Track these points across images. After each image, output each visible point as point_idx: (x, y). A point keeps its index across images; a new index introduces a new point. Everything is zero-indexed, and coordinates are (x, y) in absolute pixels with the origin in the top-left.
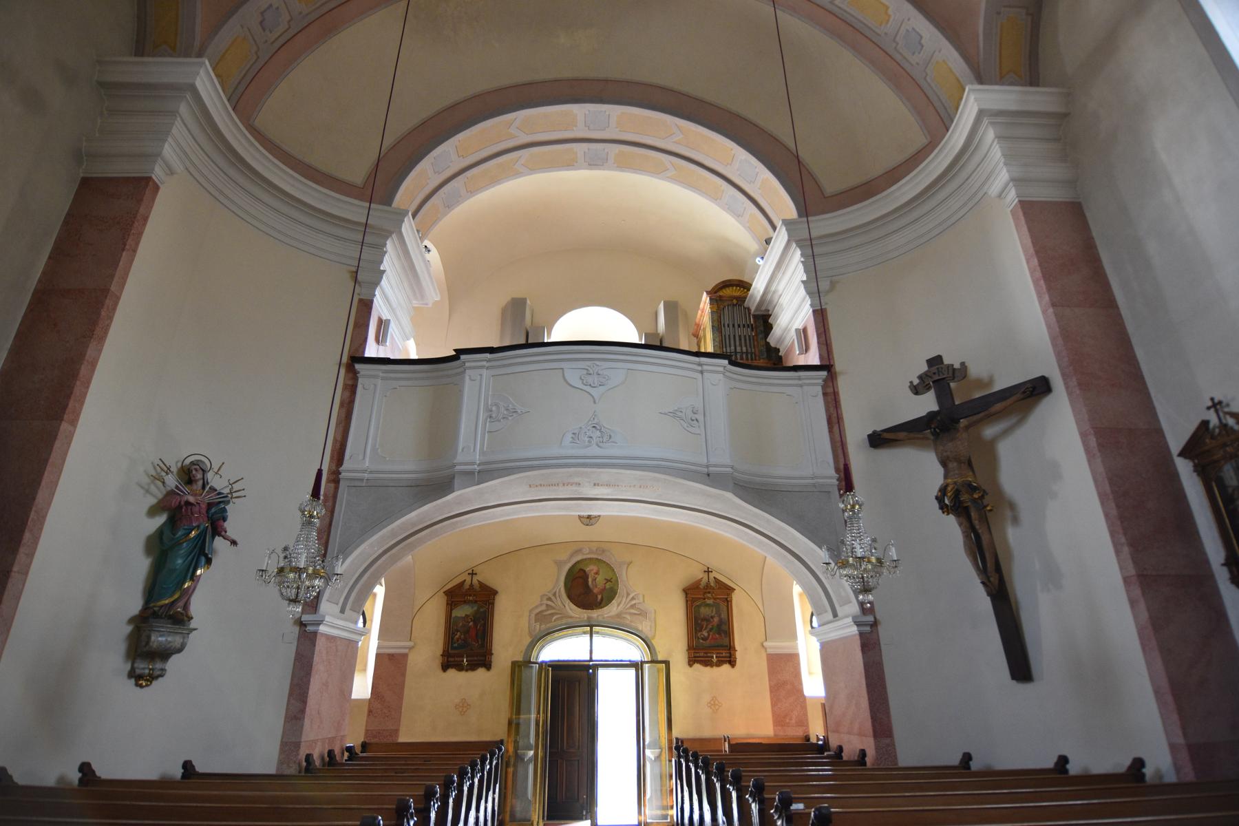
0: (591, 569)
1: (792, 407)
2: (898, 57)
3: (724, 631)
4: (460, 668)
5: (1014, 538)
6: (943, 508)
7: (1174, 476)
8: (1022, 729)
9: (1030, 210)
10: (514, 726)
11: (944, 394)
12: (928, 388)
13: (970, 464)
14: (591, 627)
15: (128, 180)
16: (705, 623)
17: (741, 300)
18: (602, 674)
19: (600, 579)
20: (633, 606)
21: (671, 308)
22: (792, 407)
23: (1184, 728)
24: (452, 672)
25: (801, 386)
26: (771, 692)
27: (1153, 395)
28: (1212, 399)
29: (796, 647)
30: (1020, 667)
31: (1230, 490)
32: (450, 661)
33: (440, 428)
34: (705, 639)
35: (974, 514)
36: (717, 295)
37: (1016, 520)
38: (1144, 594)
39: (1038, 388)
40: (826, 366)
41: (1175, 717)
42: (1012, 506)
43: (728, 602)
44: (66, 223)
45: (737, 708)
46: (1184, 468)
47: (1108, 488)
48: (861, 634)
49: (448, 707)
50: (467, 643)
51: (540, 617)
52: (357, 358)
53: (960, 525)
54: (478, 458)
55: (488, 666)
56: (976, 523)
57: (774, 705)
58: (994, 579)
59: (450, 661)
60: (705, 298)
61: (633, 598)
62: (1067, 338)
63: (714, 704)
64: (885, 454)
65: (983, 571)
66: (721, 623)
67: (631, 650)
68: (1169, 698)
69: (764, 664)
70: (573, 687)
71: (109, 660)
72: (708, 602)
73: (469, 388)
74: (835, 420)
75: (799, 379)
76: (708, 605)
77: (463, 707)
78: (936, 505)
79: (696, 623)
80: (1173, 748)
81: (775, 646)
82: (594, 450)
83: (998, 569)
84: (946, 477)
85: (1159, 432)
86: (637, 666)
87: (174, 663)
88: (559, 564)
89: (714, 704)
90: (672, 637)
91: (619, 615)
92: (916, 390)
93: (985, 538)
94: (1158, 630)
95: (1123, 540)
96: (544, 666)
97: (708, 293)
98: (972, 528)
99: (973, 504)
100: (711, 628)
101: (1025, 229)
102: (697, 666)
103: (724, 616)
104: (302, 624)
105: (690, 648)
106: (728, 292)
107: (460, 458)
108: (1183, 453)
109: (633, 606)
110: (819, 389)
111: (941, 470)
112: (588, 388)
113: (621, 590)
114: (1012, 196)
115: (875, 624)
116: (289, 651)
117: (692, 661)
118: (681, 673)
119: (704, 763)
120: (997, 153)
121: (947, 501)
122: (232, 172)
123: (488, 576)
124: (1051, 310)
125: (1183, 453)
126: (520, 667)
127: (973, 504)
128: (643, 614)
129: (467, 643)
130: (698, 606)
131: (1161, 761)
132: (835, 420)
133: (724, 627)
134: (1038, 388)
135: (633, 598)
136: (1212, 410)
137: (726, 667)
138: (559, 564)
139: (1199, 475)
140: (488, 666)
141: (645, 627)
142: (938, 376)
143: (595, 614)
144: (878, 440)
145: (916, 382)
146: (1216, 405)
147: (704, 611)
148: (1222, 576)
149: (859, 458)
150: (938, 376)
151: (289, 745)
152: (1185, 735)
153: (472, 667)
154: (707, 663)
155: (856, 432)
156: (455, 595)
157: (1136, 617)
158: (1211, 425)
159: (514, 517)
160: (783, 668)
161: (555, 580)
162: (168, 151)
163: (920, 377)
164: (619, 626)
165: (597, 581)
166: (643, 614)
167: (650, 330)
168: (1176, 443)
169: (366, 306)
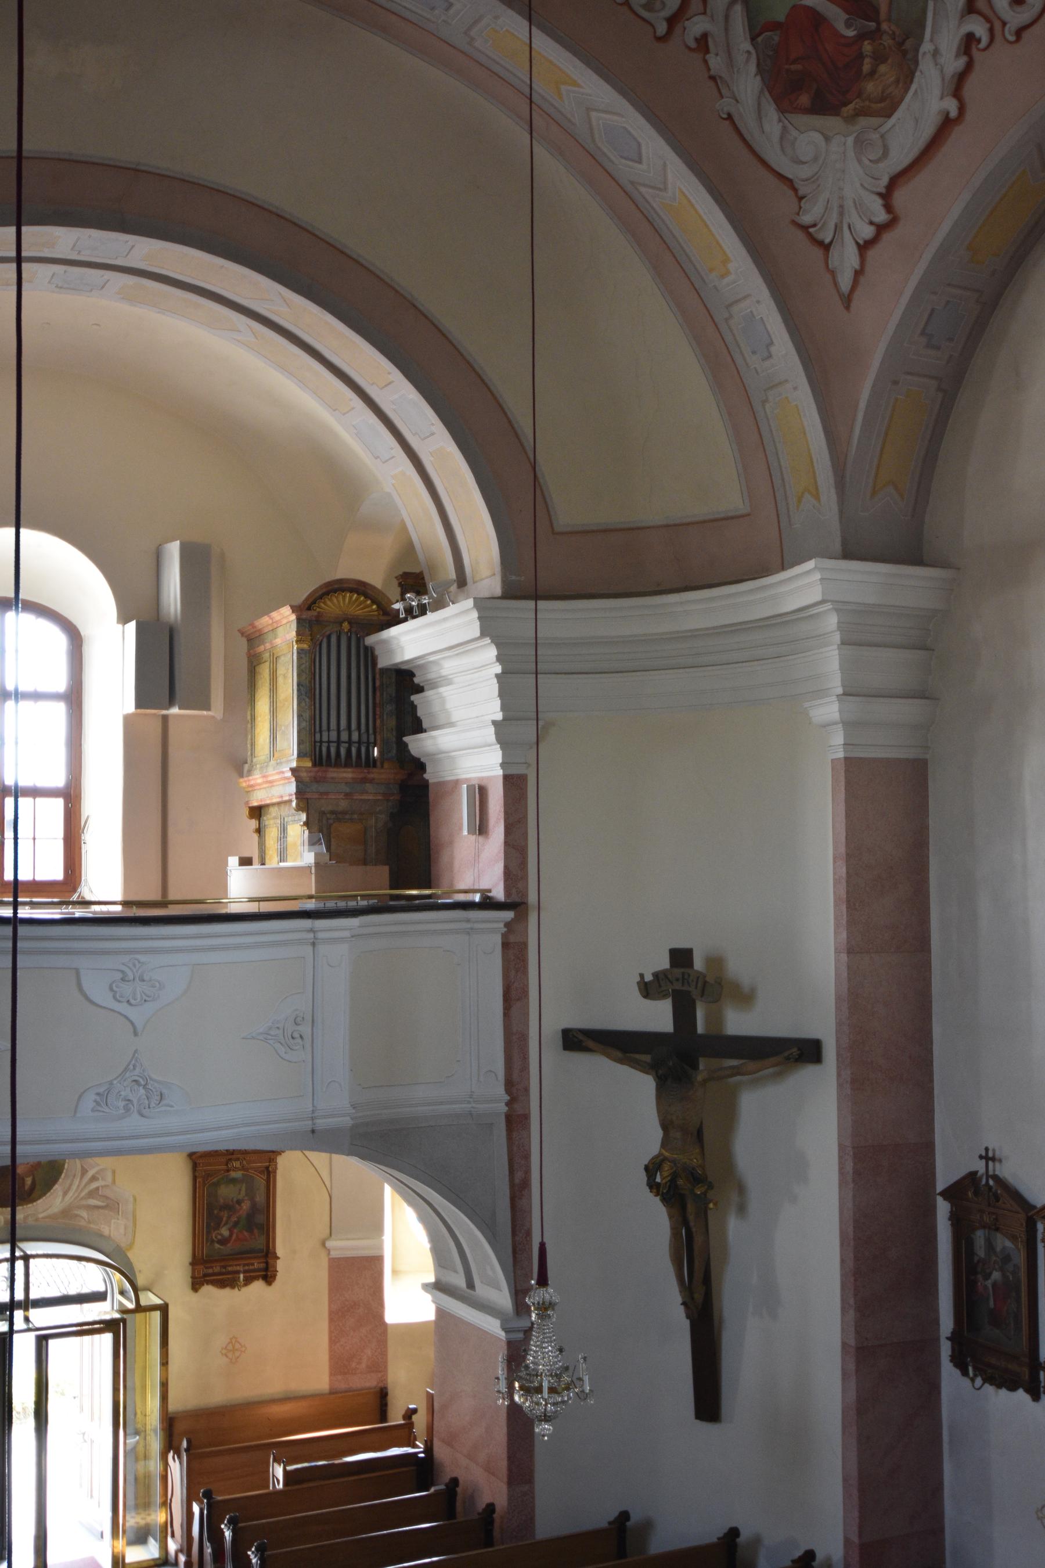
1: (448, 964)
2: (729, 338)
3: (260, 1222)
5: (736, 1231)
6: (652, 1185)
7: (932, 1210)
8: (695, 1482)
9: (856, 773)
11: (683, 1013)
12: (661, 996)
13: (699, 1134)
16: (225, 1215)
20: (93, 1194)
21: (196, 560)
23: (861, 1527)
25: (469, 932)
26: (331, 1320)
27: (936, 1092)
28: (987, 1149)
29: (381, 1247)
30: (708, 1404)
31: (976, 1259)
34: (223, 1242)
35: (690, 1208)
37: (742, 1209)
38: (857, 1371)
39: (808, 1051)
41: (856, 1514)
42: (741, 1189)
45: (271, 1346)
46: (943, 1208)
47: (850, 1230)
48: (510, 1343)
53: (671, 1217)
56: (691, 1218)
57: (333, 1341)
58: (699, 1297)
61: (94, 1178)
62: (854, 1000)
63: (233, 1349)
65: (687, 1289)
66: (254, 1209)
68: (855, 1492)
72: (233, 1174)
75: (468, 921)
76: (234, 1181)
78: (643, 1177)
79: (210, 1213)
80: (847, 1541)
81: (342, 1246)
82: (134, 1123)
83: (707, 1280)
84: (664, 1145)
85: (929, 1147)
89: (233, 1349)
91: (66, 1213)
92: (649, 989)
93: (698, 1239)
94: (864, 1411)
95: (852, 1301)
97: (294, 609)
98: (685, 1223)
99: (692, 1187)
100: (232, 1227)
101: (842, 796)
102: (208, 1289)
103: (260, 1198)
105: (196, 1261)
108: (946, 1194)
109: (93, 1194)
110: (498, 939)
111: (660, 1133)
112: (123, 1008)
114: (836, 744)
117: (196, 1285)
119: (207, 1442)
121: (658, 1179)
124: (844, 957)
125: (946, 1194)
127: (692, 1187)
128: (112, 1206)
130: (217, 1185)
132: (514, 995)
133: (260, 1218)
134: (808, 1051)
135: (94, 1178)
136: (984, 1161)
137: (258, 1285)
139: (952, 1225)
141: (114, 1229)
142: (682, 979)
144: (574, 1040)
145: (648, 978)
146: (988, 1157)
147: (227, 1192)
148: (946, 1349)
150: (682, 979)
152: (860, 1536)
154: (226, 1281)
157: (844, 1391)
158: (979, 1174)
160: (357, 1281)
163: (656, 975)
164: (64, 1231)
166: (112, 1206)
168: (945, 1177)
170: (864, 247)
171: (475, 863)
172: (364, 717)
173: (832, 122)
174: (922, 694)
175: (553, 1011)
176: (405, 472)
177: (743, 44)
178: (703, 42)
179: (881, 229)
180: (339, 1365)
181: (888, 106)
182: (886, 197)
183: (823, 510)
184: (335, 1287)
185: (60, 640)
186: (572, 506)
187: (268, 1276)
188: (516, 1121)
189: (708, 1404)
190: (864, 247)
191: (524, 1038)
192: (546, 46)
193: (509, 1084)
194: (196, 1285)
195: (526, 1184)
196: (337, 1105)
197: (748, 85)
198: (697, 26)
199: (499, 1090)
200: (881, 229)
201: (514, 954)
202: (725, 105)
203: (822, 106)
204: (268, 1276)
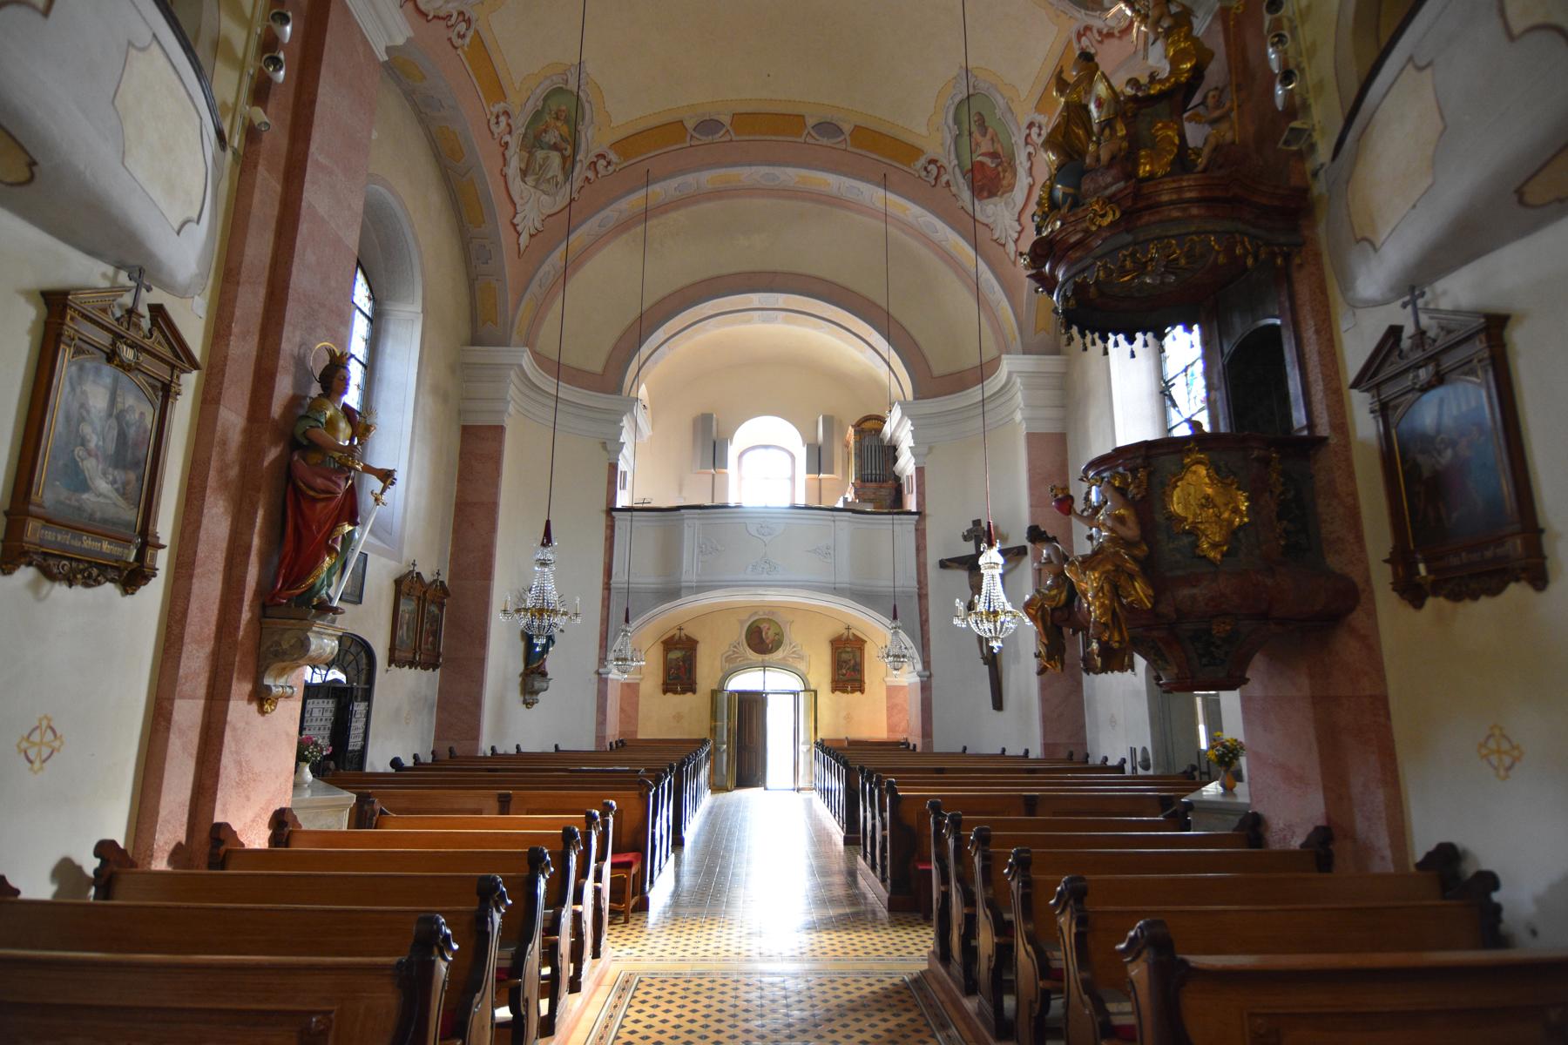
0: (764, 626)
4: (675, 692)
9: (1032, 438)
10: (713, 730)
14: (765, 667)
15: (490, 427)
17: (879, 431)
18: (770, 697)
19: (771, 633)
21: (829, 421)
22: (892, 538)
24: (669, 695)
30: (998, 704)
32: (668, 688)
33: (670, 554)
36: (859, 428)
40: (920, 513)
43: (861, 650)
44: (461, 458)
45: (873, 716)
49: (664, 717)
50: (679, 673)
51: (728, 659)
52: (611, 509)
54: (695, 578)
55: (694, 691)
59: (668, 688)
60: (851, 431)
63: (848, 718)
64: (948, 573)
67: (795, 683)
69: (884, 694)
70: (751, 707)
71: (515, 696)
73: (687, 533)
74: (920, 548)
77: (678, 717)
82: (764, 576)
86: (795, 694)
87: (541, 696)
88: (742, 622)
89: (848, 718)
90: (821, 675)
92: (966, 538)
96: (732, 693)
100: (848, 670)
104: (599, 674)
105: (833, 681)
106: (868, 425)
107: (684, 578)
113: (786, 641)
114: (1023, 431)
115: (930, 676)
116: (593, 688)
117: (833, 690)
118: (826, 698)
120: (1019, 398)
122: (532, 394)
123: (690, 631)
126: (715, 694)
129: (679, 673)
131: (1036, 752)
132: (920, 548)
138: (742, 622)
140: (694, 691)
141: (802, 666)
143: (767, 657)
144: (944, 564)
147: (845, 656)
149: (933, 571)
151: (600, 737)
153: (684, 692)
154: (844, 691)
155: (933, 556)
156: (669, 644)
159: (713, 606)
161: (740, 634)
162: (511, 409)
164: (783, 666)
165: (769, 635)
166: (801, 658)
167: (812, 441)
169: (613, 467)
170: (1016, 241)
171: (911, 503)
172: (876, 457)
173: (996, 199)
174: (1063, 407)
175: (933, 556)
176: (856, 352)
177: (961, 180)
178: (948, 183)
179: (1020, 233)
180: (891, 728)
181: (1011, 187)
182: (1019, 220)
183: (1018, 343)
184: (889, 697)
185: (789, 459)
186: (939, 368)
187: (862, 691)
188: (922, 596)
189: (998, 704)
190: (1016, 241)
191: (925, 565)
192: (892, 197)
193: (919, 582)
194: (833, 690)
195: (927, 620)
196: (844, 578)
197: (966, 195)
198: (944, 178)
199: (915, 583)
200: (1020, 233)
201: (920, 534)
202: (960, 203)
203: (992, 194)
204: (862, 691)
